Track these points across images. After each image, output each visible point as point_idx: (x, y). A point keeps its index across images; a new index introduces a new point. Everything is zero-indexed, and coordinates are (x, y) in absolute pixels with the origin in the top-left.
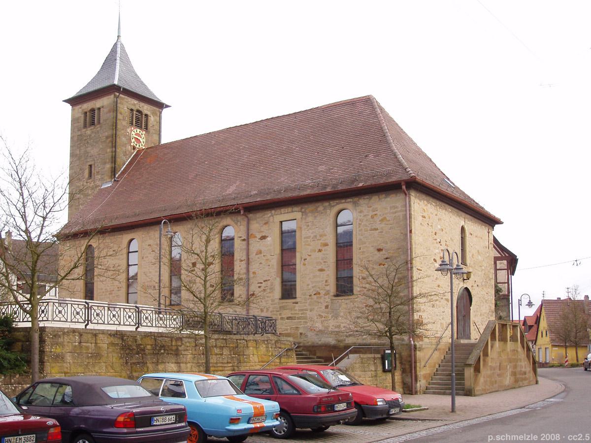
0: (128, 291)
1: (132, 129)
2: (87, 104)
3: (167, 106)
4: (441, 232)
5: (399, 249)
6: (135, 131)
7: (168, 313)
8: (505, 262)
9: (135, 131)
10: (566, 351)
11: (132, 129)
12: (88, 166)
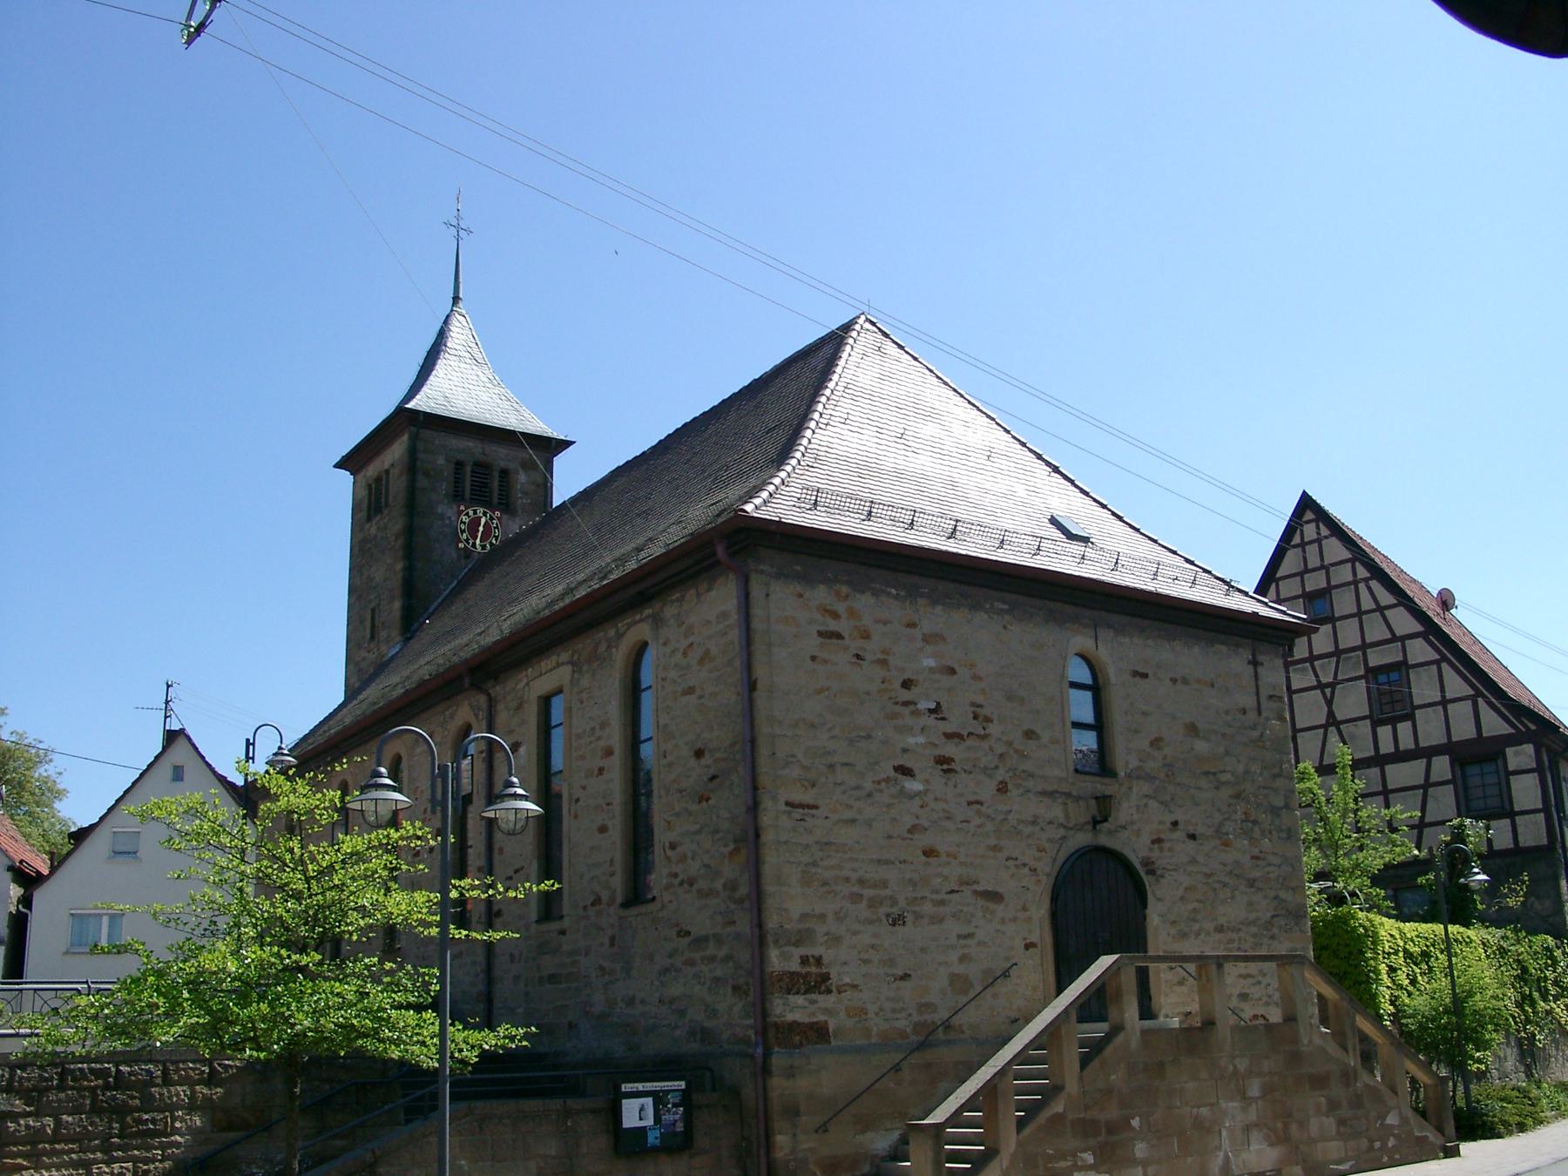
0: (1101, 741)
1: (462, 508)
2: (372, 465)
3: (565, 444)
4: (1181, 826)
5: (735, 743)
6: (471, 513)
7: (477, 912)
8: (1529, 748)
9: (471, 513)
10: (1096, 632)
11: (462, 508)
12: (370, 611)
